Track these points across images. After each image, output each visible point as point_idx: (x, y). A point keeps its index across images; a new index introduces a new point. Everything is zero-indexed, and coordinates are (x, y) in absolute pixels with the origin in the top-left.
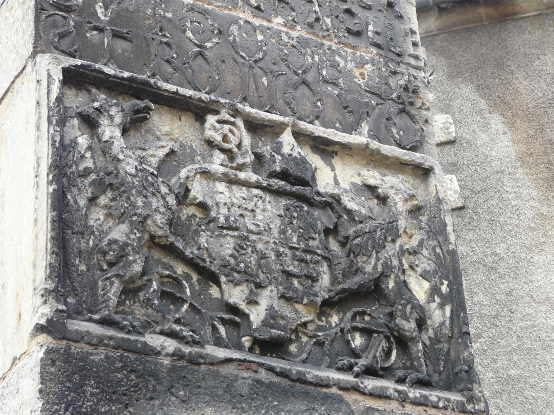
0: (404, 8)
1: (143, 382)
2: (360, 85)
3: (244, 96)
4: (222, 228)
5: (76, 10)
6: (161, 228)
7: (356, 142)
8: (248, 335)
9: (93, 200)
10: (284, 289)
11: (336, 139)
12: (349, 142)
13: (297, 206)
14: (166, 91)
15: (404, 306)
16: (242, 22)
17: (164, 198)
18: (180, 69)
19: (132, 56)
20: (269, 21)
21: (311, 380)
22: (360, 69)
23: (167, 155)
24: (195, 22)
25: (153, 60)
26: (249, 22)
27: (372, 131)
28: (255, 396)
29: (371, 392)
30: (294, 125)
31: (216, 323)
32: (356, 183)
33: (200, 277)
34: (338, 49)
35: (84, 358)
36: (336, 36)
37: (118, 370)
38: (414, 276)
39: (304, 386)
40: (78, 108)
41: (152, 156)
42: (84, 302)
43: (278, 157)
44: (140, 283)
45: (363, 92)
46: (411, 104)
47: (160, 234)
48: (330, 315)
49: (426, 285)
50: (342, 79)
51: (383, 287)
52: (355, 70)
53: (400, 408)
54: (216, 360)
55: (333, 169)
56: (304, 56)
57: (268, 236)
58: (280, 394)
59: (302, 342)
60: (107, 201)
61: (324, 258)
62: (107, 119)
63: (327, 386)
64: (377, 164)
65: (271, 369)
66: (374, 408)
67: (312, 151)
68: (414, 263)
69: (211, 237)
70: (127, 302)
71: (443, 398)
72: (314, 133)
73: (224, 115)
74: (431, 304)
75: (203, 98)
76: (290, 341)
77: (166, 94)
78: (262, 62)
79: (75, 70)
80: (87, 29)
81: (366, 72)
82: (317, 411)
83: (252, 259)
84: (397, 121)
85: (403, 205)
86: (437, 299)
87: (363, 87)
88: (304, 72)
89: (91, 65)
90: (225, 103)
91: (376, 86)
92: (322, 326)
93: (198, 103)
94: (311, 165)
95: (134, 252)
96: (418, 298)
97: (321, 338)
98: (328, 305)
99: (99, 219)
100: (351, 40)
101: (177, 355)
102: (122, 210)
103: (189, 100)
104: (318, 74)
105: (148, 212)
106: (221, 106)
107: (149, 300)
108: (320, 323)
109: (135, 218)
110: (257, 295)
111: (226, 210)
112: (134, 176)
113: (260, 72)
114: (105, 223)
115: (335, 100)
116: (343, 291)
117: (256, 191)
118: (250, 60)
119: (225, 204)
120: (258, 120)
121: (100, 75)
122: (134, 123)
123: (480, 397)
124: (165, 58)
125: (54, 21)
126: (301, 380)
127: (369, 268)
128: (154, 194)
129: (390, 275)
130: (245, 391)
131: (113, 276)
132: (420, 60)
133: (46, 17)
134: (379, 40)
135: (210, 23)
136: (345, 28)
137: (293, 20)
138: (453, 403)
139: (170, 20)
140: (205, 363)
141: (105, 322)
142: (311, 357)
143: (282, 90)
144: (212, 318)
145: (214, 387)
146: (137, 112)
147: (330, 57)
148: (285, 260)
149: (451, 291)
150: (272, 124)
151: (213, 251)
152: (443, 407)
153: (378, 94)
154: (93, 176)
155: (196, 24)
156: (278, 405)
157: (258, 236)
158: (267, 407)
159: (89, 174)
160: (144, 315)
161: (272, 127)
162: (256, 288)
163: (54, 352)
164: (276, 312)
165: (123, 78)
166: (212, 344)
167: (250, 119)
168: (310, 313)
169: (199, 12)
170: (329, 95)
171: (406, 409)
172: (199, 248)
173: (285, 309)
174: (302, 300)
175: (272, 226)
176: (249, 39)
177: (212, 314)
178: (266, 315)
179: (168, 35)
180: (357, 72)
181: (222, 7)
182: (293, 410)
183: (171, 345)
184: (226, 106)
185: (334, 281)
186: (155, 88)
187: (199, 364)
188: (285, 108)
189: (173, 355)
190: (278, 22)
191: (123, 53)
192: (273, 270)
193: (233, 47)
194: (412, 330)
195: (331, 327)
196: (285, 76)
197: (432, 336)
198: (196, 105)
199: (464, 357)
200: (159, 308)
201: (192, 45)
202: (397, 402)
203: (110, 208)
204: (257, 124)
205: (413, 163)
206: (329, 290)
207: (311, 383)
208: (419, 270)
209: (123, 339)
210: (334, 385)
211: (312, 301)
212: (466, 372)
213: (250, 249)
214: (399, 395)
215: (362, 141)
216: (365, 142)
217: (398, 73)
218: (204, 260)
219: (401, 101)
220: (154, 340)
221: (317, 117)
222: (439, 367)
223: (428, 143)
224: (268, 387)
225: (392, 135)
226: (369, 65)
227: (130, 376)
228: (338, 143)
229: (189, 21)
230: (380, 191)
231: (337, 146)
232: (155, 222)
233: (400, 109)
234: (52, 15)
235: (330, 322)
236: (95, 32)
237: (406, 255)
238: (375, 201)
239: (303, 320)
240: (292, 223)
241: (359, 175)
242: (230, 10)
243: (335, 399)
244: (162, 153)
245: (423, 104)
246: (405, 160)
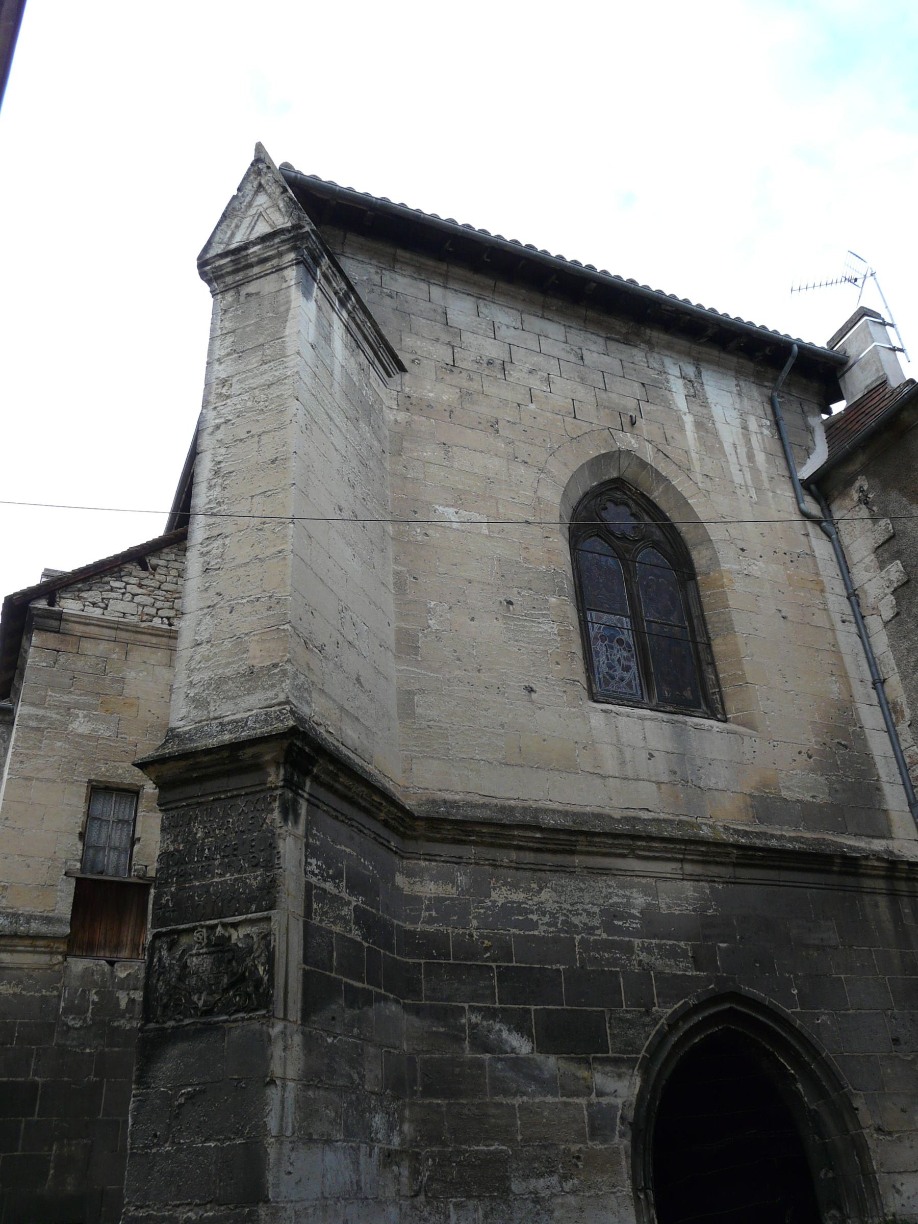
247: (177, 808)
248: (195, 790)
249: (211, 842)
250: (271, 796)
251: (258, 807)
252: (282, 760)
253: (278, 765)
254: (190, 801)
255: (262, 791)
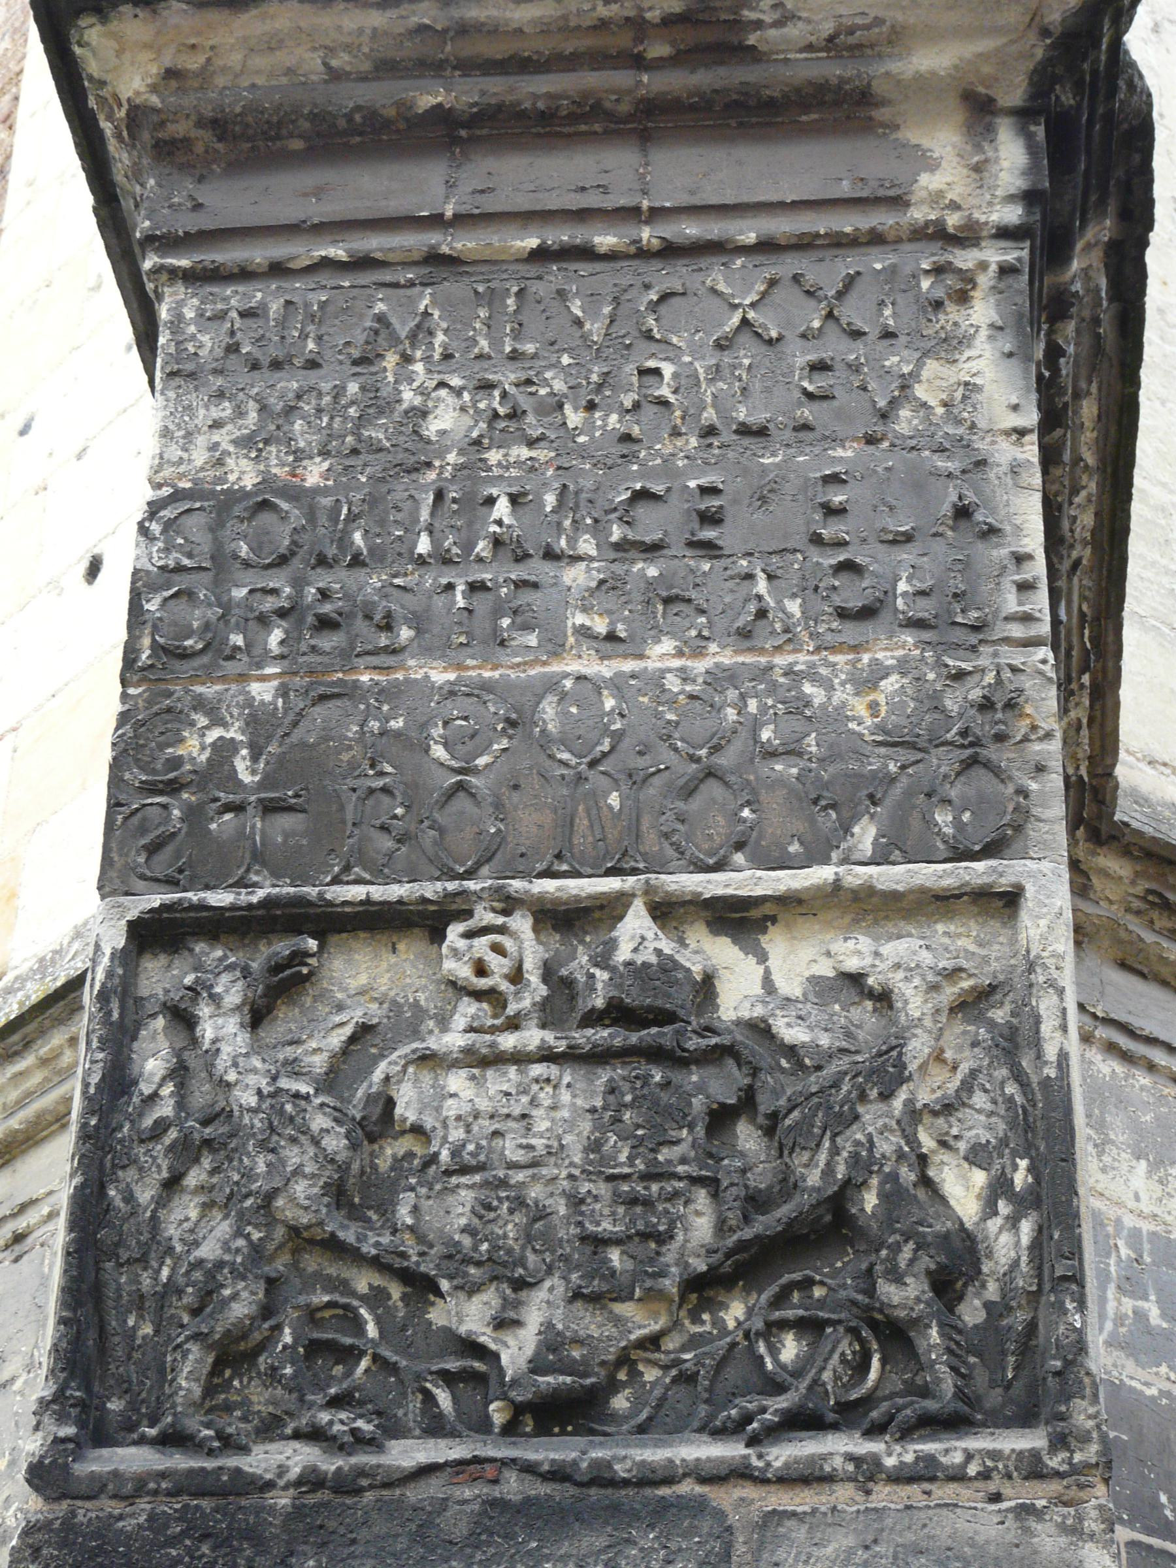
1: (226, 1555)
2: (861, 735)
4: (448, 1173)
6: (306, 1208)
7: (807, 884)
8: (497, 1399)
9: (172, 1184)
10: (581, 1277)
11: (758, 892)
13: (636, 1077)
14: (345, 903)
15: (896, 1249)
16: (568, 684)
17: (316, 1142)
19: (305, 842)
20: (641, 656)
21: (625, 1475)
23: (353, 1039)
26: (585, 678)
28: (484, 1537)
29: (780, 1474)
30: (649, 890)
31: (428, 1385)
32: (820, 977)
33: (408, 1289)
34: (812, 665)
35: (104, 1527)
37: (173, 1541)
38: (955, 1163)
39: (609, 1491)
40: (167, 991)
41: (316, 1051)
42: (143, 1401)
43: (602, 975)
44: (257, 1336)
47: (305, 1221)
48: (724, 1306)
49: (979, 1178)
50: (814, 735)
51: (853, 1211)
52: (853, 701)
53: (857, 1498)
54: (396, 1476)
55: (762, 958)
56: (719, 711)
57: (556, 1165)
58: (547, 1522)
59: (644, 1384)
60: (204, 1176)
61: (695, 1181)
62: (208, 1005)
63: (669, 1480)
64: (883, 914)
65: (529, 1469)
66: (785, 1512)
67: (711, 932)
68: (947, 1133)
69: (429, 1197)
70: (236, 1383)
71: (979, 1451)
72: (701, 894)
73: (484, 916)
74: (990, 1223)
76: (613, 1386)
77: (348, 910)
81: (882, 699)
82: (635, 1543)
83: (510, 1226)
85: (926, 1001)
86: (1004, 1207)
87: (868, 738)
88: (716, 749)
89: (180, 899)
90: (483, 889)
92: (701, 1335)
94: (688, 970)
95: (233, 1278)
96: (960, 1214)
97: (687, 1365)
98: (703, 1289)
99: (187, 1219)
100: (851, 632)
101: (311, 1480)
102: (228, 1191)
103: (399, 907)
105: (277, 1183)
107: (274, 1369)
108: (698, 1329)
109: (249, 1202)
110: (517, 1305)
111: (462, 1130)
112: (254, 1111)
113: (604, 781)
114: (202, 1224)
116: (742, 1246)
117: (537, 1070)
119: (459, 1118)
120: (565, 904)
122: (278, 992)
123: (1089, 1432)
124: (378, 823)
125: (144, 819)
126: (602, 1478)
127: (814, 1178)
128: (293, 1140)
129: (865, 1183)
130: (461, 1530)
131: (188, 1339)
133: (126, 819)
134: (924, 609)
135: (492, 709)
137: (700, 636)
138: (1008, 1458)
139: (398, 734)
140: (371, 1487)
141: (174, 1439)
142: (663, 1412)
143: (657, 807)
144: (418, 1377)
145: (388, 1535)
146: (276, 969)
148: (593, 1211)
149: (1038, 1180)
150: (598, 903)
151: (430, 1229)
152: (979, 1473)
153: (908, 742)
154: (173, 1134)
156: (538, 1548)
157: (530, 1172)
158: (512, 1557)
159: (165, 1131)
160: (268, 1402)
162: (515, 1290)
163: (39, 1529)
164: (559, 1334)
165: (250, 907)
166: (417, 1432)
167: (549, 906)
168: (655, 1315)
171: (873, 1497)
172: (395, 1231)
173: (591, 1324)
174: (633, 1293)
175: (567, 1139)
176: (587, 713)
177: (421, 1366)
178: (537, 1346)
179: (389, 769)
180: (860, 707)
181: (525, 663)
182: (574, 1552)
183: (298, 1457)
184: (485, 895)
185: (721, 1228)
187: (359, 1491)
188: (661, 849)
189: (298, 1483)
191: (285, 841)
192: (561, 1240)
194: (910, 1303)
195: (724, 1332)
196: (667, 773)
197: (995, 1298)
199: (1057, 1339)
200: (292, 1384)
201: (441, 772)
202: (852, 1484)
203: (212, 1188)
204: (567, 911)
205: (968, 889)
206: (708, 1251)
207: (626, 1483)
208: (962, 1146)
209: (191, 1472)
210: (685, 1475)
211: (650, 1289)
212: (1058, 1374)
213: (506, 1205)
214: (856, 1467)
216: (831, 878)
217: (970, 673)
218: (403, 1255)
220: (262, 1459)
221: (739, 846)
222: (1004, 1369)
224: (519, 1512)
226: (894, 678)
227: (198, 1549)
228: (764, 899)
230: (870, 981)
231: (768, 905)
232: (293, 1199)
233: (962, 761)
234: (137, 810)
235: (724, 1321)
236: (228, 817)
237: (927, 1119)
238: (869, 1004)
239: (633, 1337)
240: (620, 1121)
241: (828, 954)
242: (544, 663)
243: (687, 1508)
244: (336, 1040)
245: (1034, 728)
246: (944, 890)
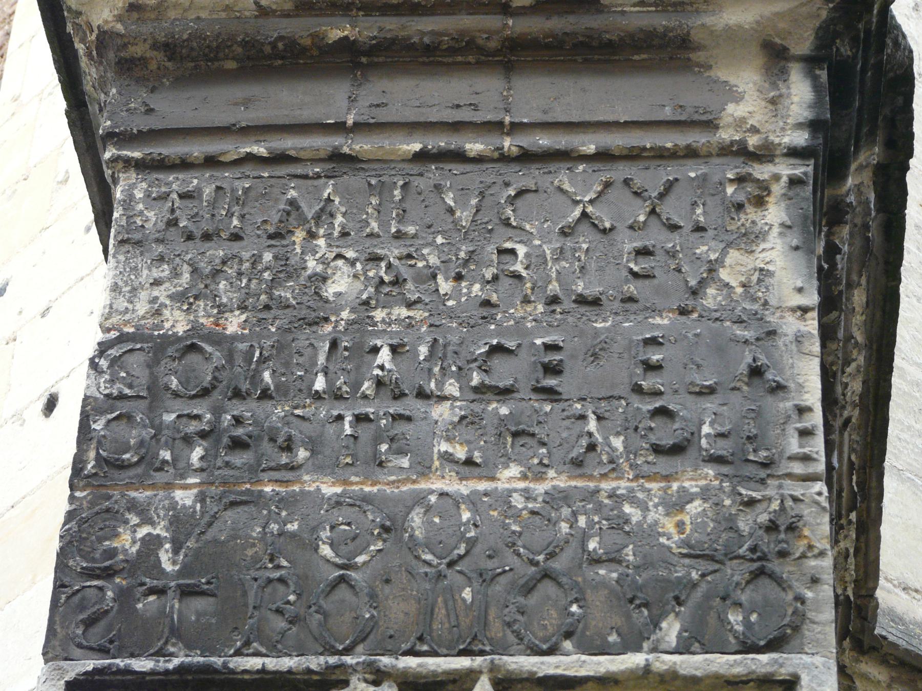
0: (792, 367)
2: (669, 548)
3: (419, 635)
5: (124, 568)
7: (623, 667)
11: (583, 673)
12: (608, 672)
14: (245, 672)
18: (302, 617)
19: (214, 621)
20: (493, 479)
22: (676, 515)
24: (342, 524)
25: (250, 618)
26: (447, 494)
27: (686, 631)
36: (631, 465)
45: (675, 559)
46: (783, 554)
50: (631, 547)
56: (555, 524)
72: (536, 673)
75: (313, 667)
77: (246, 677)
78: (466, 561)
79: (86, 680)
80: (138, 595)
84: (744, 598)
88: (551, 556)
89: (110, 665)
90: (358, 663)
91: (706, 539)
93: (306, 677)
100: (663, 464)
103: (288, 676)
104: (581, 551)
106: (350, 671)
113: (460, 579)
115: (612, 591)
118: (440, 564)
120: (425, 677)
121: (129, 677)
124: (274, 607)
132: (815, 460)
133: (68, 598)
134: (723, 448)
135: (371, 517)
136: (647, 446)
137: (541, 463)
139: (293, 535)
143: (502, 601)
147: (612, 510)
150: (451, 677)
155: (343, 527)
161: (454, 681)
167: (411, 679)
169: (351, 505)
170: (603, 584)
176: (447, 523)
180: (669, 525)
181: (399, 481)
184: (359, 668)
186: (225, 673)
190: (509, 476)
191: (198, 620)
193: (410, 548)
196: (511, 574)
198: (305, 681)
201: (328, 567)
205: (754, 677)
215: (637, 662)
217: (759, 501)
219: (758, 554)
221: (568, 635)
223: (814, 623)
225: (729, 627)
226: (697, 503)
229: (328, 528)
233: (751, 572)
234: (78, 591)
236: (152, 598)
245: (810, 547)
246: (734, 676)
247: (211, 162)
248: (332, 99)
249: (410, 324)
250: (740, 180)
251: (670, 210)
252: (803, 45)
253: (776, 57)
254: (289, 143)
255: (691, 153)
